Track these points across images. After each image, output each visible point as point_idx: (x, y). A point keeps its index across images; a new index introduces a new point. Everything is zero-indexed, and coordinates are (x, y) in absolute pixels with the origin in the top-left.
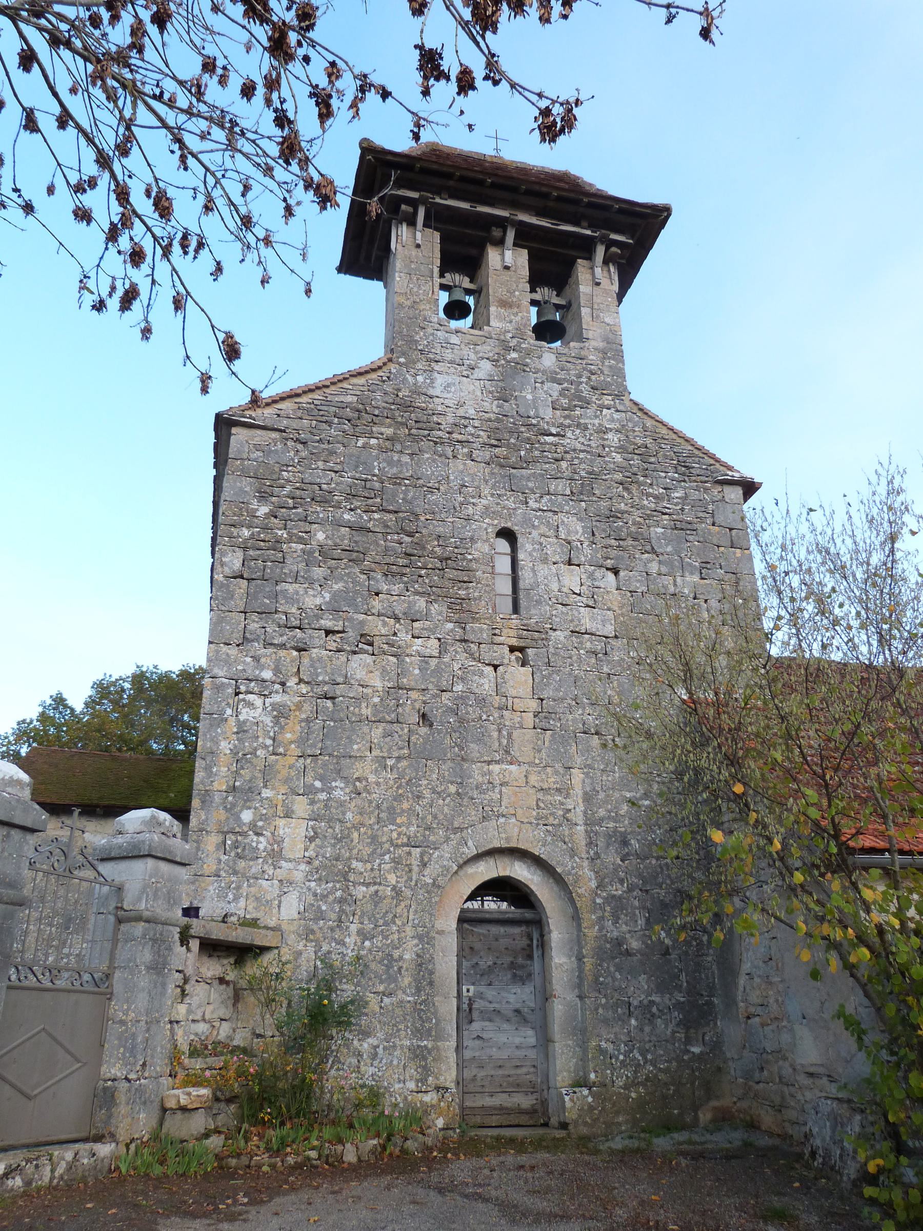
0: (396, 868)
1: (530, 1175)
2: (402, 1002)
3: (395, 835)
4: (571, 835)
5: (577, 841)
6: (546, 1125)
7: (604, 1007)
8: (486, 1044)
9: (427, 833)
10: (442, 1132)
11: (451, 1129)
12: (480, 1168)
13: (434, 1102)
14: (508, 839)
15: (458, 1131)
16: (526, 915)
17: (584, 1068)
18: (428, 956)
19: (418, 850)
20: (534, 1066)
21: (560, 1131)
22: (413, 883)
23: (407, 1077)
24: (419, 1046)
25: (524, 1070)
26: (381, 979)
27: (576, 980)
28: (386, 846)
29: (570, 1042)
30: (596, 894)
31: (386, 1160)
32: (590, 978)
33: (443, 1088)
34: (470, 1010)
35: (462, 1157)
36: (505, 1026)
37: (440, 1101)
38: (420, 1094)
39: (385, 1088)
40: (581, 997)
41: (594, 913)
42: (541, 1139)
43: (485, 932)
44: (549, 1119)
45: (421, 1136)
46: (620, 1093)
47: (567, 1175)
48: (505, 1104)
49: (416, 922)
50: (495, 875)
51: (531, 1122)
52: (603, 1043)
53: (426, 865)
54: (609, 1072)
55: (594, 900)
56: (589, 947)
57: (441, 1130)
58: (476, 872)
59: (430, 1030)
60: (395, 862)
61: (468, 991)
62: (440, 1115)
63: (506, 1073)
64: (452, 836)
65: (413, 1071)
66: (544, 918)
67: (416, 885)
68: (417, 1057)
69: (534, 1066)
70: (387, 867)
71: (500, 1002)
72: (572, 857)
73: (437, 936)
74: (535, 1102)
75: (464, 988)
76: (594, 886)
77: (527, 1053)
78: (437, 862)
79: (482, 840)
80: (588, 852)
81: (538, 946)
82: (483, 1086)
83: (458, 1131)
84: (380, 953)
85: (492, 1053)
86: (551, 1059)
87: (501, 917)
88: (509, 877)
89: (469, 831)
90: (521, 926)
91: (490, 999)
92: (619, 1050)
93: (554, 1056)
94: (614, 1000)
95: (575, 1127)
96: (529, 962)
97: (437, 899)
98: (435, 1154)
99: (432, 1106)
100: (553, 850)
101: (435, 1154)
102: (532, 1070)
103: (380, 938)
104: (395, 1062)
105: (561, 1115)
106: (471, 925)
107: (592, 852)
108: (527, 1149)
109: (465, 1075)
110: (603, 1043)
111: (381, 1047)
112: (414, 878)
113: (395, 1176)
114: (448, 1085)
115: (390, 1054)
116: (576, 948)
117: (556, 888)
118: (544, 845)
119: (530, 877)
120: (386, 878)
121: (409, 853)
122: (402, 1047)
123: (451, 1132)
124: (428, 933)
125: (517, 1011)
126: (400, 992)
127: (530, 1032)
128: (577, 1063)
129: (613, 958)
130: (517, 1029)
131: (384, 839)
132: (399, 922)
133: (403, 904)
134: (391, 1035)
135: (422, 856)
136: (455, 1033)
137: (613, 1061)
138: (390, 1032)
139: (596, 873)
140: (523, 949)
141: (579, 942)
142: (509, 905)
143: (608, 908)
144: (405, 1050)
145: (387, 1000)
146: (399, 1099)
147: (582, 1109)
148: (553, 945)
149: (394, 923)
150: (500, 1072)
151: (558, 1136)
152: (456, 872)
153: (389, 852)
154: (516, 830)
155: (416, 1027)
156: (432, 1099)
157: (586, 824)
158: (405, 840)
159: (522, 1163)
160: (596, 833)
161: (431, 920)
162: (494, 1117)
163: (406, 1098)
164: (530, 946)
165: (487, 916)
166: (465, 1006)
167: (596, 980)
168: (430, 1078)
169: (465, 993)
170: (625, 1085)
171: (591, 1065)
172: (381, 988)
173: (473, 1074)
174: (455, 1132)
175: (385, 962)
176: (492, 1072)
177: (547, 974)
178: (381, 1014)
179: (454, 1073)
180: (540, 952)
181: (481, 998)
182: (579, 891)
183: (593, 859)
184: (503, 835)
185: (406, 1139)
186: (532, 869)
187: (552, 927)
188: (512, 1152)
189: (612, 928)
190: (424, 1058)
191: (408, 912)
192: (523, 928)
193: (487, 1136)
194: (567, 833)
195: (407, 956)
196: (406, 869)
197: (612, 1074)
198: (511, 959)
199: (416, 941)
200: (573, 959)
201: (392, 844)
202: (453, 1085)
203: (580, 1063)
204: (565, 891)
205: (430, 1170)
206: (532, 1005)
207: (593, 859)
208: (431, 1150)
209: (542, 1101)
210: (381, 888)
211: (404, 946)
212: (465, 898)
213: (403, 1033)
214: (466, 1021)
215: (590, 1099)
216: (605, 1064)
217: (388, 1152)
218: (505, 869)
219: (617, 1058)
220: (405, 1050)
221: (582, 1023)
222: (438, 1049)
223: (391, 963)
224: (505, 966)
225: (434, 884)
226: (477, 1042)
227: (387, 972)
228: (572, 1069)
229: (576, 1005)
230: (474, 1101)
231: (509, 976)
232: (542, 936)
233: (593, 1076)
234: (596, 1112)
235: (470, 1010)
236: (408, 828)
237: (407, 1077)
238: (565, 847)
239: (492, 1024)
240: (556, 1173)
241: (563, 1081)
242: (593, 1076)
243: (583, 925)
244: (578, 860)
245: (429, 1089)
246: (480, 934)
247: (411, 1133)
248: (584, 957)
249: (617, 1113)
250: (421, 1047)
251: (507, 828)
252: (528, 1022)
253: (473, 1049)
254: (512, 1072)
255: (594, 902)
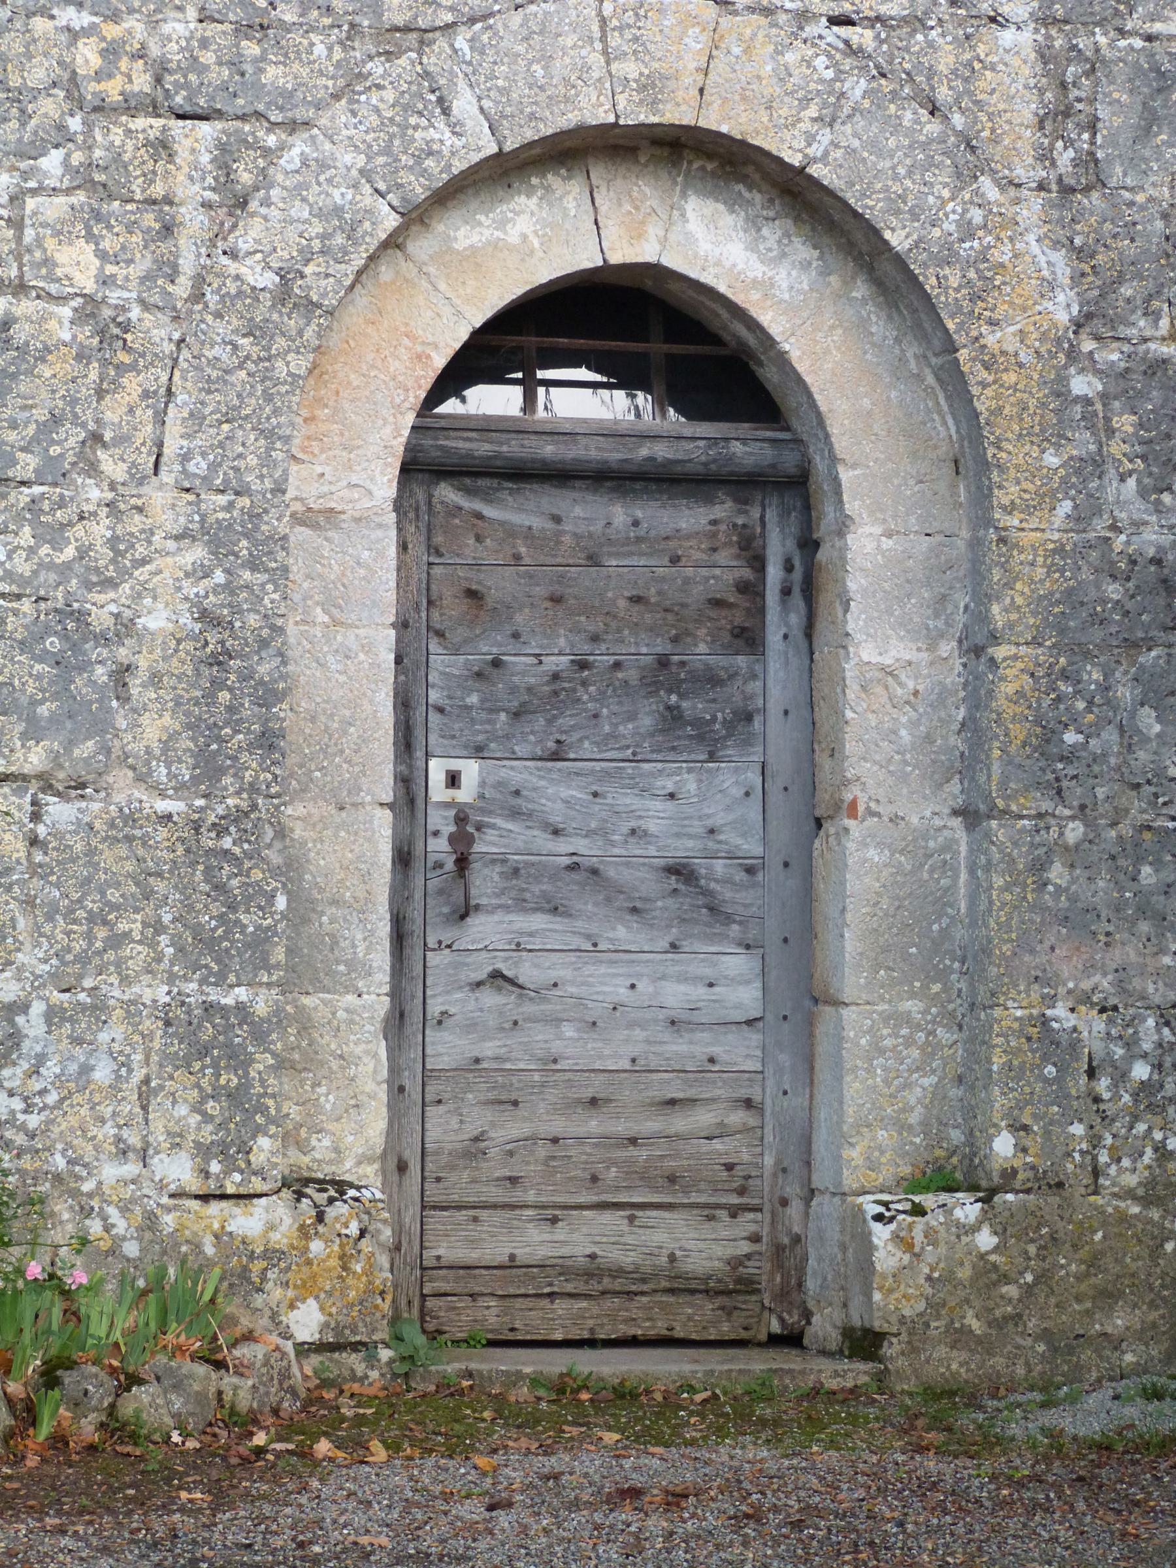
0: (97, 216)
1: (656, 1524)
2: (130, 819)
3: (88, 56)
4: (968, 72)
5: (995, 102)
6: (791, 1340)
7: (1073, 855)
8: (529, 1008)
9: (251, 49)
10: (315, 1360)
11: (355, 1347)
12: (447, 1497)
13: (279, 1239)
14: (649, 87)
15: (385, 1354)
16: (737, 448)
17: (970, 1112)
18: (253, 620)
19: (205, 129)
20: (748, 1103)
21: (845, 1364)
22: (182, 288)
23: (159, 1137)
24: (209, 1008)
25: (704, 1118)
26: (32, 720)
27: (958, 742)
28: (49, 107)
29: (913, 1006)
30: (1073, 354)
31: (32, 1461)
32: (1019, 732)
33: (322, 1184)
34: (462, 862)
35: (379, 1452)
36: (622, 933)
37: (304, 1233)
38: (215, 1207)
39: (58, 1178)
40: (970, 816)
41: (1059, 439)
42: (762, 1392)
43: (537, 522)
44: (807, 1315)
45: (201, 1369)
46: (1123, 1219)
47: (816, 1531)
48: (614, 1256)
49: (198, 466)
50: (585, 258)
51: (726, 1330)
52: (1060, 1010)
53: (243, 204)
54: (1078, 1129)
55: (1062, 380)
56: (1020, 593)
57: (304, 1350)
58: (496, 245)
59: (261, 941)
60: (89, 185)
61: (453, 780)
62: (307, 1289)
63: (622, 1128)
64: (376, 68)
65: (182, 1110)
66: (820, 465)
67: (197, 296)
68: (204, 1051)
69: (748, 1103)
70: (54, 208)
71: (601, 832)
72: (965, 176)
73: (301, 534)
74: (745, 1247)
75: (437, 770)
76: (1063, 317)
77: (716, 1050)
78: (298, 192)
79: (520, 91)
80: (1045, 157)
81: (786, 592)
82: (513, 1180)
83: (385, 1354)
84: (26, 606)
85: (557, 1047)
86: (823, 1074)
87: (614, 455)
88: (656, 270)
89: (461, 43)
90: (710, 500)
91: (556, 819)
92: (1131, 1044)
93: (838, 1064)
94: (1126, 829)
95: (913, 1350)
96: (741, 661)
97: (299, 364)
98: (260, 1439)
99: (272, 1255)
100: (874, 146)
101: (260, 1439)
102: (738, 1117)
103: (26, 536)
104: (102, 1073)
105: (856, 1302)
106: (470, 492)
107: (1065, 158)
108: (677, 1430)
109: (432, 1134)
110: (1060, 1010)
111: (38, 1008)
112: (187, 265)
113: (51, 1521)
114: (347, 1170)
115: (77, 1041)
116: (962, 599)
117: (879, 326)
118: (829, 121)
119: (756, 269)
120: (49, 262)
121: (163, 147)
122: (132, 1008)
123: (355, 1361)
124: (255, 516)
125: (680, 871)
126: (120, 778)
127: (737, 963)
128: (937, 1094)
129: (1133, 645)
130: (674, 947)
131: (37, 75)
132: (112, 466)
133: (132, 385)
134: (83, 959)
135: (225, 156)
136: (381, 959)
137: (1103, 1085)
138: (79, 945)
139: (1081, 253)
140: (717, 603)
141: (977, 574)
142: (660, 406)
143: (1125, 422)
144: (147, 1024)
145: (59, 812)
146: (121, 1226)
147: (948, 1278)
148: (854, 584)
149: (93, 469)
150: (594, 1125)
151: (832, 1384)
152: (393, 243)
153: (62, 137)
154: (695, 42)
155: (197, 931)
156: (271, 1227)
157: (1045, 20)
158: (142, 82)
159: (637, 1480)
160: (1094, 65)
161: (266, 460)
162: (560, 1306)
163: (151, 1221)
164: (752, 590)
165: (549, 450)
166: (440, 847)
167: (1049, 735)
168: (264, 1142)
169: (438, 791)
170: (1150, 1184)
171: (1000, 1102)
172: (34, 759)
173: (471, 1130)
174: (371, 1360)
175: (53, 643)
176: (557, 1126)
177: (822, 712)
178: (34, 870)
179: (376, 1124)
180: (796, 619)
181: (515, 814)
182: (991, 340)
183: (1067, 190)
184: (629, 69)
185: (135, 1380)
186: (771, 234)
187: (852, 505)
188: (611, 1437)
189: (1138, 509)
190: (238, 1060)
191: (160, 420)
192: (723, 509)
193: (516, 1378)
194: (945, 61)
195: (155, 620)
196: (149, 220)
197: (1095, 1141)
198: (661, 646)
199: (196, 554)
200: (947, 648)
201: (76, 101)
202: (370, 1174)
203: (955, 1092)
204: (923, 337)
205: (220, 1499)
206: (752, 847)
207: (1067, 190)
208: (247, 1423)
209: (779, 1249)
210: (26, 307)
211: (141, 573)
212: (440, 361)
213: (137, 954)
214: (439, 908)
215: (986, 1240)
216: (1062, 1098)
217: (45, 1430)
218: (638, 235)
219: (1121, 1076)
220: (147, 1024)
221: (973, 924)
222: (305, 1024)
223: (75, 647)
224: (631, 674)
225: (283, 294)
226: (490, 998)
227: (61, 689)
228: (914, 1118)
229: (949, 846)
230: (473, 1242)
231: (647, 722)
232: (809, 545)
233: (1003, 1145)
234: (1011, 1291)
235: (462, 862)
236: (153, 24)
237: (159, 1137)
238: (933, 128)
239: (558, 923)
240: (774, 1519)
241: (873, 1167)
242: (1003, 1145)
243: (1002, 497)
244: (992, 193)
245: (257, 1185)
246: (511, 532)
247: (161, 1359)
248: (995, 638)
249: (1107, 1297)
250: (223, 1010)
251: (649, 30)
252: (729, 919)
253: (471, 1027)
254: (652, 1125)
255: (1060, 391)
